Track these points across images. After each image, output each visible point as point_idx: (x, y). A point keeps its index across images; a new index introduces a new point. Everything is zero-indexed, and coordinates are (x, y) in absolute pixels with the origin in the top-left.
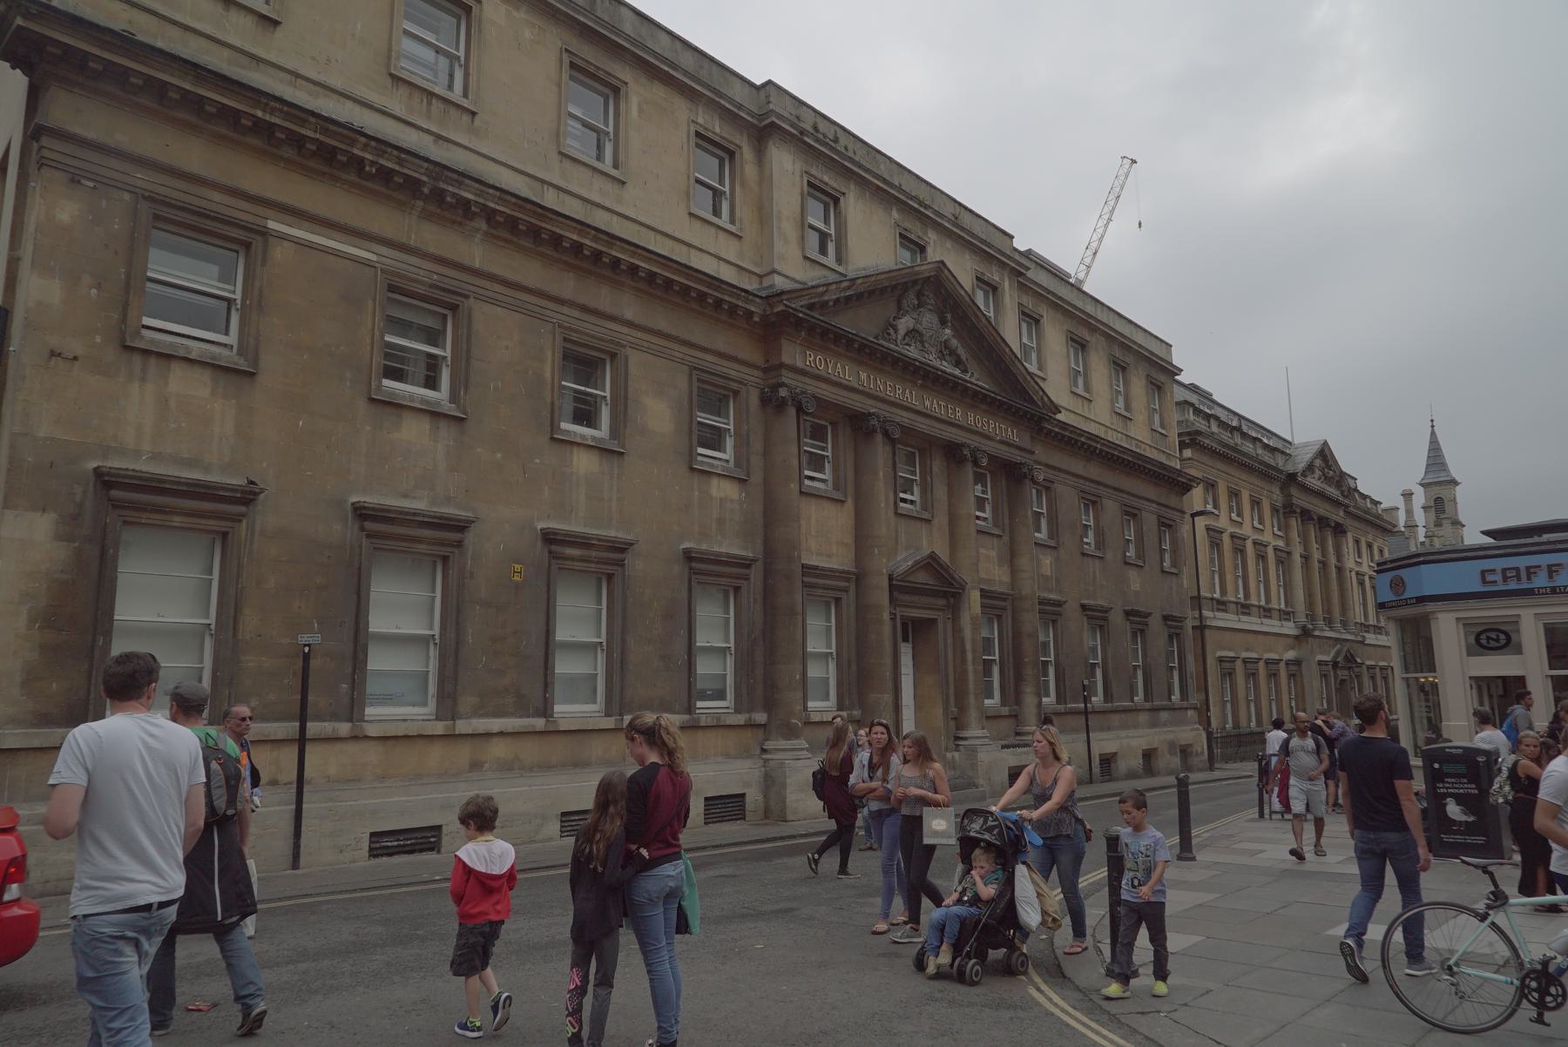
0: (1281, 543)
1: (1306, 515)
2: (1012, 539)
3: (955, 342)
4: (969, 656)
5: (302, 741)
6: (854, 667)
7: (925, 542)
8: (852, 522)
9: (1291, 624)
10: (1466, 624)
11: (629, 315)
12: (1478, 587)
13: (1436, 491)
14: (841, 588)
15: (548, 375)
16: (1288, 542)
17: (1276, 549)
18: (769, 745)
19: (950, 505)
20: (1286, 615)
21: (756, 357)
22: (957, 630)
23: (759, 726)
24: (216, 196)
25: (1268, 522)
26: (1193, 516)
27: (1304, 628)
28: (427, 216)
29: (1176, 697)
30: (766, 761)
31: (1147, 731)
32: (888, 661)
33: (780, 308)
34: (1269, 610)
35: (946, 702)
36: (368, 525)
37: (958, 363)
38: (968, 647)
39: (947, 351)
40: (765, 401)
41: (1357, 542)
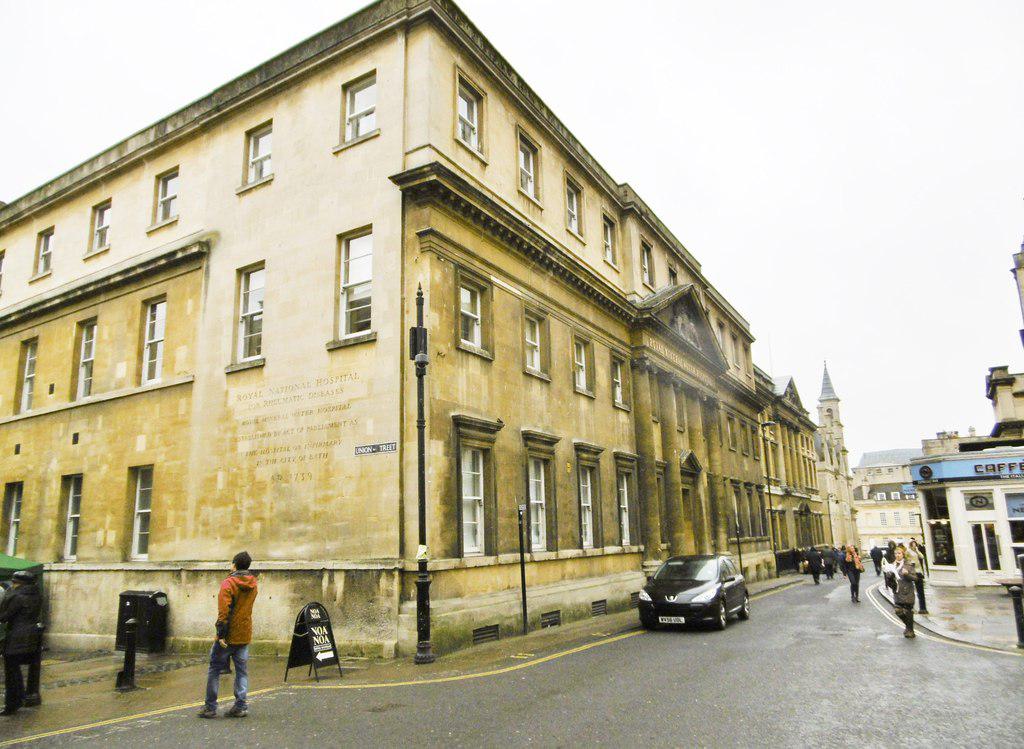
0: (772, 439)
3: (694, 331)
5: (523, 563)
10: (966, 494)
12: (972, 474)
13: (827, 405)
16: (776, 438)
18: (646, 563)
21: (626, 339)
24: (477, 263)
26: (764, 426)
28: (535, 269)
29: (588, 542)
30: (646, 572)
31: (756, 554)
36: (530, 443)
38: (703, 505)
39: (694, 338)
40: (633, 367)
41: (802, 437)
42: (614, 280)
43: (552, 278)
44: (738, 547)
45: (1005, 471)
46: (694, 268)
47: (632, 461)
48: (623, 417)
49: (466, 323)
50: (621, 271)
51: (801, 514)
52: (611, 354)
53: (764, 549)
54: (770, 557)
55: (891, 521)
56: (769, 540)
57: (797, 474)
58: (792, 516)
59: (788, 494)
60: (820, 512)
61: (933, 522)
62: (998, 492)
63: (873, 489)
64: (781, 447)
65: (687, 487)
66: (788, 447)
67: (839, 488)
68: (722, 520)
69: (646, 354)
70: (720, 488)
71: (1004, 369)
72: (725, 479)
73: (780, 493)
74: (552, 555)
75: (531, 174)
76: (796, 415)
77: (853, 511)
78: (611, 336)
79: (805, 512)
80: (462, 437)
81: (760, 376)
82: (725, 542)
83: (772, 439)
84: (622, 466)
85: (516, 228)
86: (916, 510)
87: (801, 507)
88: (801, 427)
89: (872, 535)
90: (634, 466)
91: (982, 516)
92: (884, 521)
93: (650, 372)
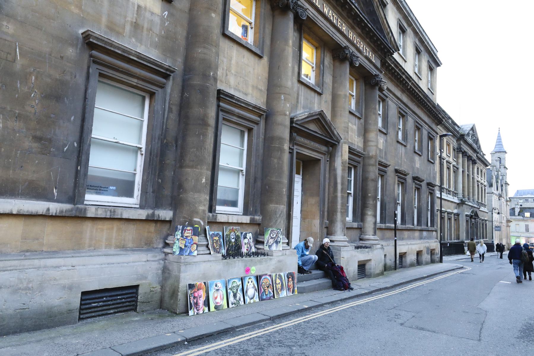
0: (455, 163)
1: (464, 154)
2: (366, 121)
4: (339, 187)
6: (259, 183)
7: (316, 105)
8: (266, 75)
14: (253, 120)
17: (453, 166)
19: (333, 88)
20: (455, 194)
22: (332, 169)
23: (164, 222)
25: (452, 154)
26: (441, 136)
27: (462, 200)
30: (166, 254)
31: (419, 241)
32: (285, 181)
34: (450, 191)
35: (322, 217)
38: (339, 180)
41: (478, 168)
46: (434, 52)
51: (471, 217)
54: (435, 245)
56: (436, 231)
57: (471, 191)
58: (465, 217)
60: (486, 219)
63: (523, 210)
64: (461, 170)
66: (467, 173)
67: (501, 206)
73: (457, 201)
74: (494, 227)
77: (508, 221)
79: (474, 216)
83: (455, 163)
88: (478, 161)
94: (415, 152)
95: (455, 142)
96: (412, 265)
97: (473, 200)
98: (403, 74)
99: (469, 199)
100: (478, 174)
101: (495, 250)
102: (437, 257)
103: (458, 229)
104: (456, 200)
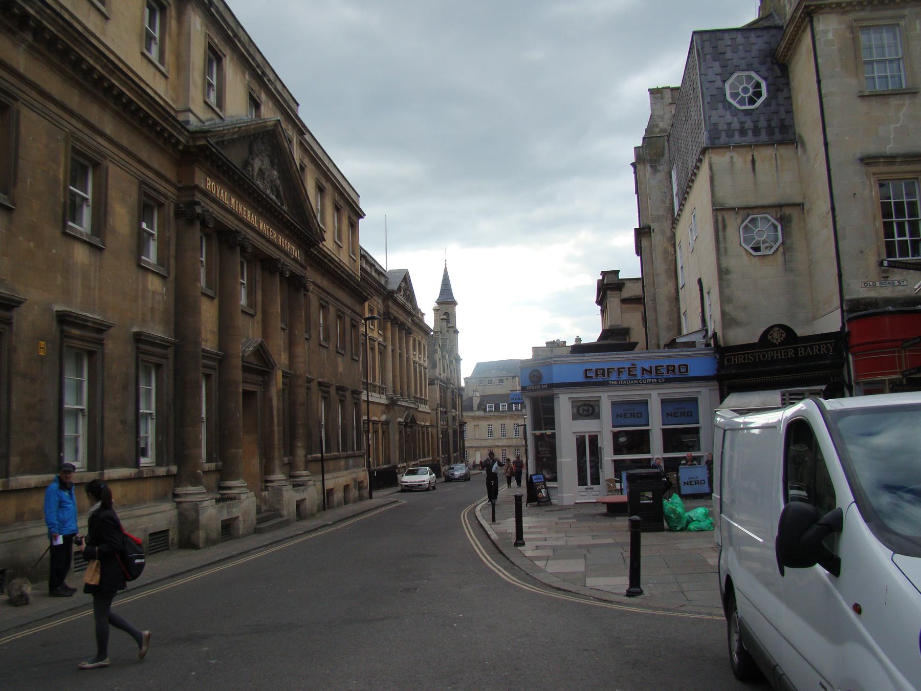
0: (381, 339)
3: (278, 182)
9: (384, 397)
11: (108, 131)
12: (580, 378)
15: (61, 177)
16: (385, 340)
17: (379, 344)
18: (180, 490)
20: (382, 390)
21: (170, 174)
22: (267, 400)
30: (179, 503)
31: (345, 473)
33: (202, 142)
34: (375, 386)
37: (278, 196)
38: (275, 413)
40: (178, 214)
41: (414, 340)
42: (158, 87)
43: (31, 47)
44: (322, 466)
45: (614, 377)
47: (166, 347)
48: (154, 284)
49: (72, 209)
50: (172, 75)
51: (406, 425)
52: (140, 188)
53: (356, 466)
54: (363, 475)
55: (497, 433)
58: (397, 426)
59: (392, 405)
60: (427, 424)
61: (538, 432)
62: (605, 399)
65: (250, 388)
68: (300, 431)
69: (199, 197)
70: (301, 392)
71: (616, 273)
72: (309, 381)
75: (157, 35)
76: (409, 313)
78: (140, 161)
80: (66, 337)
81: (367, 261)
82: (303, 459)
83: (381, 339)
84: (146, 353)
85: (104, 66)
86: (521, 422)
87: (406, 418)
88: (414, 328)
89: (478, 448)
90: (170, 355)
91: (587, 426)
92: (490, 433)
93: (204, 224)
94: (338, 352)
95: (380, 302)
96: (339, 505)
97: (409, 396)
98: (326, 257)
99: (402, 395)
100: (414, 350)
101: (549, 432)
102: (366, 493)
103: (387, 448)
104: (383, 400)
